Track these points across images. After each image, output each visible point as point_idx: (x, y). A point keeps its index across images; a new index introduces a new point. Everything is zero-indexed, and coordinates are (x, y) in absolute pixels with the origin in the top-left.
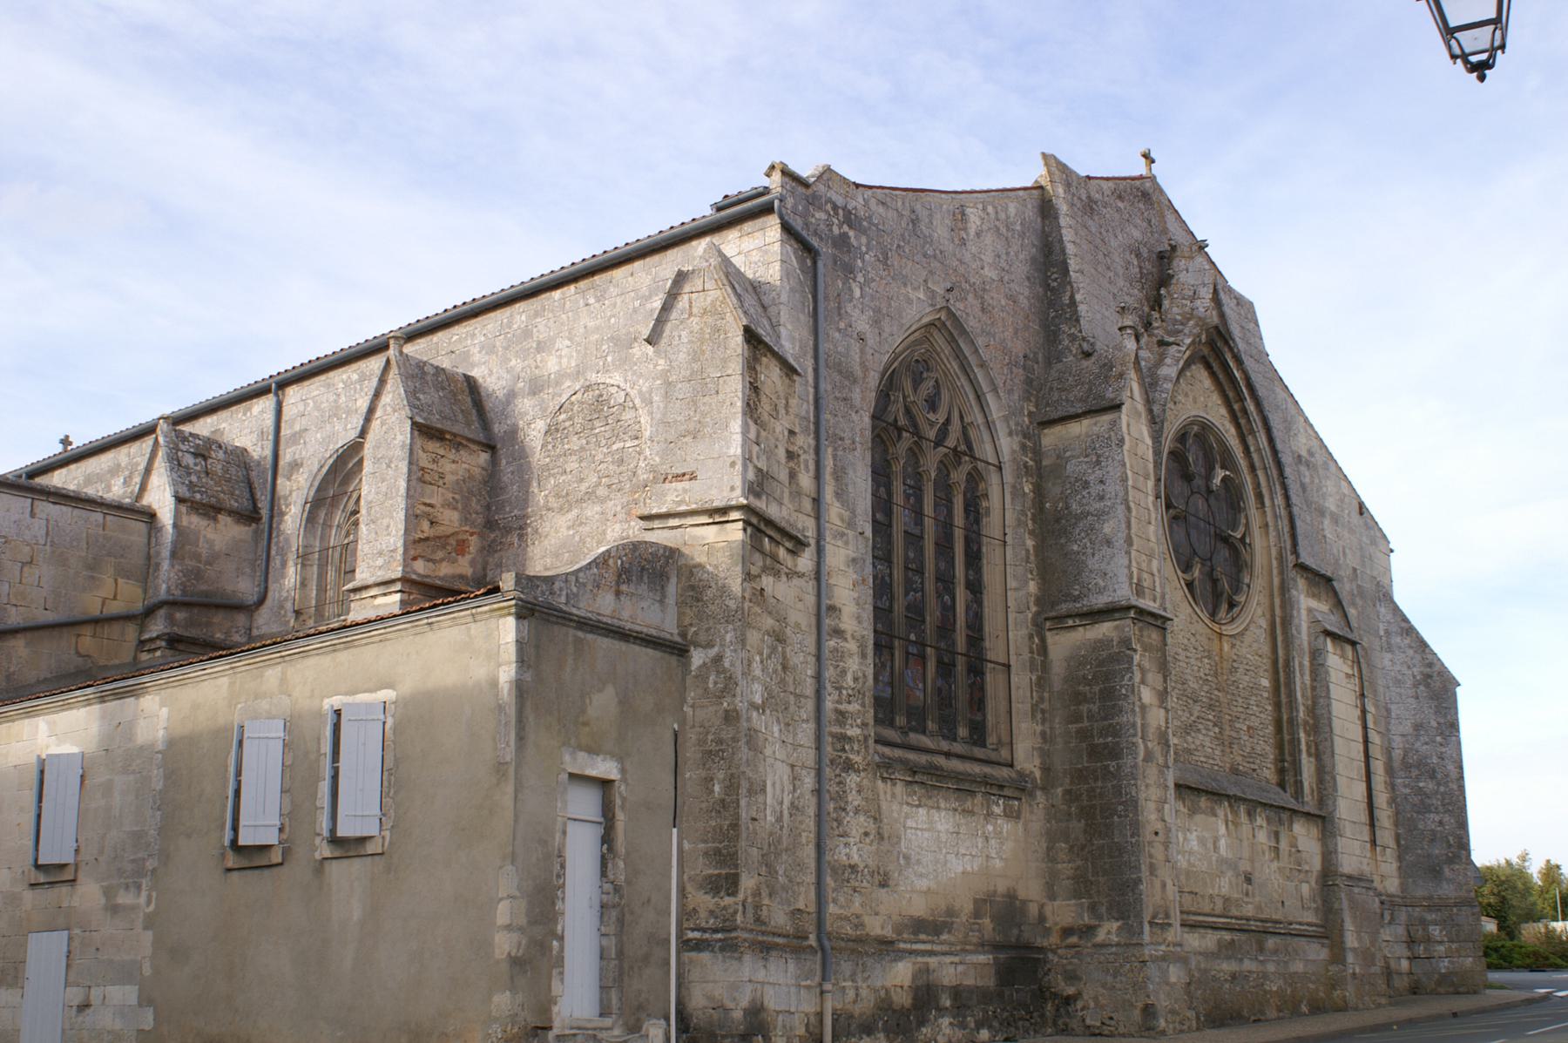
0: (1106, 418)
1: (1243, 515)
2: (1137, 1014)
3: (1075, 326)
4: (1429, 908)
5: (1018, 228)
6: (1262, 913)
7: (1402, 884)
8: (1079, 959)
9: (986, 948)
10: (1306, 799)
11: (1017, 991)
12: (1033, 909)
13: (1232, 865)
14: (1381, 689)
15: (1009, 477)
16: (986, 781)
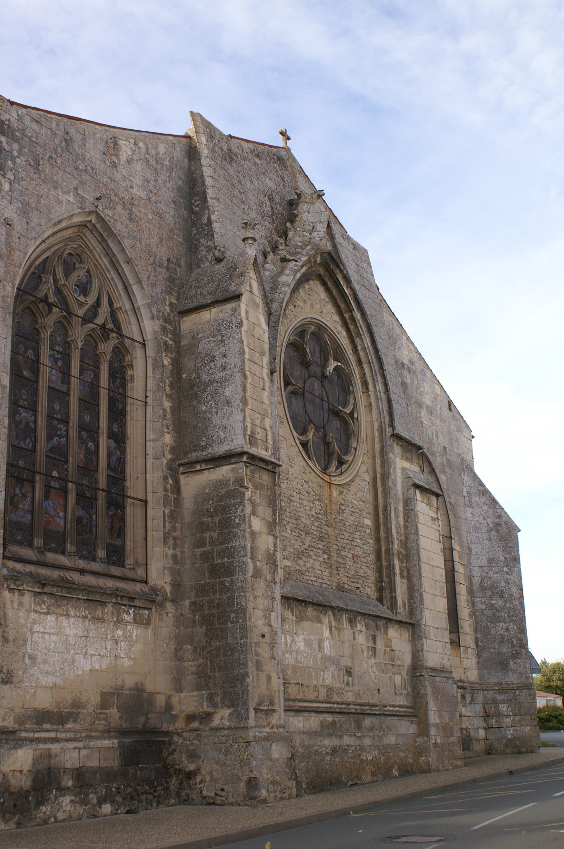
0: (229, 306)
1: (352, 396)
2: (242, 786)
3: (211, 240)
4: (500, 691)
5: (167, 163)
6: (361, 698)
7: (479, 674)
8: (199, 741)
9: (112, 734)
10: (399, 610)
11: (141, 769)
12: (161, 700)
13: (335, 662)
14: (465, 534)
15: (151, 352)
16: (116, 594)
